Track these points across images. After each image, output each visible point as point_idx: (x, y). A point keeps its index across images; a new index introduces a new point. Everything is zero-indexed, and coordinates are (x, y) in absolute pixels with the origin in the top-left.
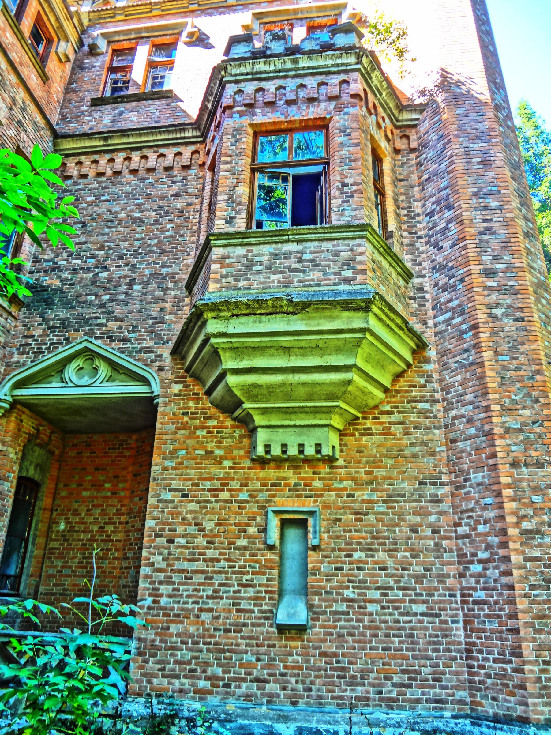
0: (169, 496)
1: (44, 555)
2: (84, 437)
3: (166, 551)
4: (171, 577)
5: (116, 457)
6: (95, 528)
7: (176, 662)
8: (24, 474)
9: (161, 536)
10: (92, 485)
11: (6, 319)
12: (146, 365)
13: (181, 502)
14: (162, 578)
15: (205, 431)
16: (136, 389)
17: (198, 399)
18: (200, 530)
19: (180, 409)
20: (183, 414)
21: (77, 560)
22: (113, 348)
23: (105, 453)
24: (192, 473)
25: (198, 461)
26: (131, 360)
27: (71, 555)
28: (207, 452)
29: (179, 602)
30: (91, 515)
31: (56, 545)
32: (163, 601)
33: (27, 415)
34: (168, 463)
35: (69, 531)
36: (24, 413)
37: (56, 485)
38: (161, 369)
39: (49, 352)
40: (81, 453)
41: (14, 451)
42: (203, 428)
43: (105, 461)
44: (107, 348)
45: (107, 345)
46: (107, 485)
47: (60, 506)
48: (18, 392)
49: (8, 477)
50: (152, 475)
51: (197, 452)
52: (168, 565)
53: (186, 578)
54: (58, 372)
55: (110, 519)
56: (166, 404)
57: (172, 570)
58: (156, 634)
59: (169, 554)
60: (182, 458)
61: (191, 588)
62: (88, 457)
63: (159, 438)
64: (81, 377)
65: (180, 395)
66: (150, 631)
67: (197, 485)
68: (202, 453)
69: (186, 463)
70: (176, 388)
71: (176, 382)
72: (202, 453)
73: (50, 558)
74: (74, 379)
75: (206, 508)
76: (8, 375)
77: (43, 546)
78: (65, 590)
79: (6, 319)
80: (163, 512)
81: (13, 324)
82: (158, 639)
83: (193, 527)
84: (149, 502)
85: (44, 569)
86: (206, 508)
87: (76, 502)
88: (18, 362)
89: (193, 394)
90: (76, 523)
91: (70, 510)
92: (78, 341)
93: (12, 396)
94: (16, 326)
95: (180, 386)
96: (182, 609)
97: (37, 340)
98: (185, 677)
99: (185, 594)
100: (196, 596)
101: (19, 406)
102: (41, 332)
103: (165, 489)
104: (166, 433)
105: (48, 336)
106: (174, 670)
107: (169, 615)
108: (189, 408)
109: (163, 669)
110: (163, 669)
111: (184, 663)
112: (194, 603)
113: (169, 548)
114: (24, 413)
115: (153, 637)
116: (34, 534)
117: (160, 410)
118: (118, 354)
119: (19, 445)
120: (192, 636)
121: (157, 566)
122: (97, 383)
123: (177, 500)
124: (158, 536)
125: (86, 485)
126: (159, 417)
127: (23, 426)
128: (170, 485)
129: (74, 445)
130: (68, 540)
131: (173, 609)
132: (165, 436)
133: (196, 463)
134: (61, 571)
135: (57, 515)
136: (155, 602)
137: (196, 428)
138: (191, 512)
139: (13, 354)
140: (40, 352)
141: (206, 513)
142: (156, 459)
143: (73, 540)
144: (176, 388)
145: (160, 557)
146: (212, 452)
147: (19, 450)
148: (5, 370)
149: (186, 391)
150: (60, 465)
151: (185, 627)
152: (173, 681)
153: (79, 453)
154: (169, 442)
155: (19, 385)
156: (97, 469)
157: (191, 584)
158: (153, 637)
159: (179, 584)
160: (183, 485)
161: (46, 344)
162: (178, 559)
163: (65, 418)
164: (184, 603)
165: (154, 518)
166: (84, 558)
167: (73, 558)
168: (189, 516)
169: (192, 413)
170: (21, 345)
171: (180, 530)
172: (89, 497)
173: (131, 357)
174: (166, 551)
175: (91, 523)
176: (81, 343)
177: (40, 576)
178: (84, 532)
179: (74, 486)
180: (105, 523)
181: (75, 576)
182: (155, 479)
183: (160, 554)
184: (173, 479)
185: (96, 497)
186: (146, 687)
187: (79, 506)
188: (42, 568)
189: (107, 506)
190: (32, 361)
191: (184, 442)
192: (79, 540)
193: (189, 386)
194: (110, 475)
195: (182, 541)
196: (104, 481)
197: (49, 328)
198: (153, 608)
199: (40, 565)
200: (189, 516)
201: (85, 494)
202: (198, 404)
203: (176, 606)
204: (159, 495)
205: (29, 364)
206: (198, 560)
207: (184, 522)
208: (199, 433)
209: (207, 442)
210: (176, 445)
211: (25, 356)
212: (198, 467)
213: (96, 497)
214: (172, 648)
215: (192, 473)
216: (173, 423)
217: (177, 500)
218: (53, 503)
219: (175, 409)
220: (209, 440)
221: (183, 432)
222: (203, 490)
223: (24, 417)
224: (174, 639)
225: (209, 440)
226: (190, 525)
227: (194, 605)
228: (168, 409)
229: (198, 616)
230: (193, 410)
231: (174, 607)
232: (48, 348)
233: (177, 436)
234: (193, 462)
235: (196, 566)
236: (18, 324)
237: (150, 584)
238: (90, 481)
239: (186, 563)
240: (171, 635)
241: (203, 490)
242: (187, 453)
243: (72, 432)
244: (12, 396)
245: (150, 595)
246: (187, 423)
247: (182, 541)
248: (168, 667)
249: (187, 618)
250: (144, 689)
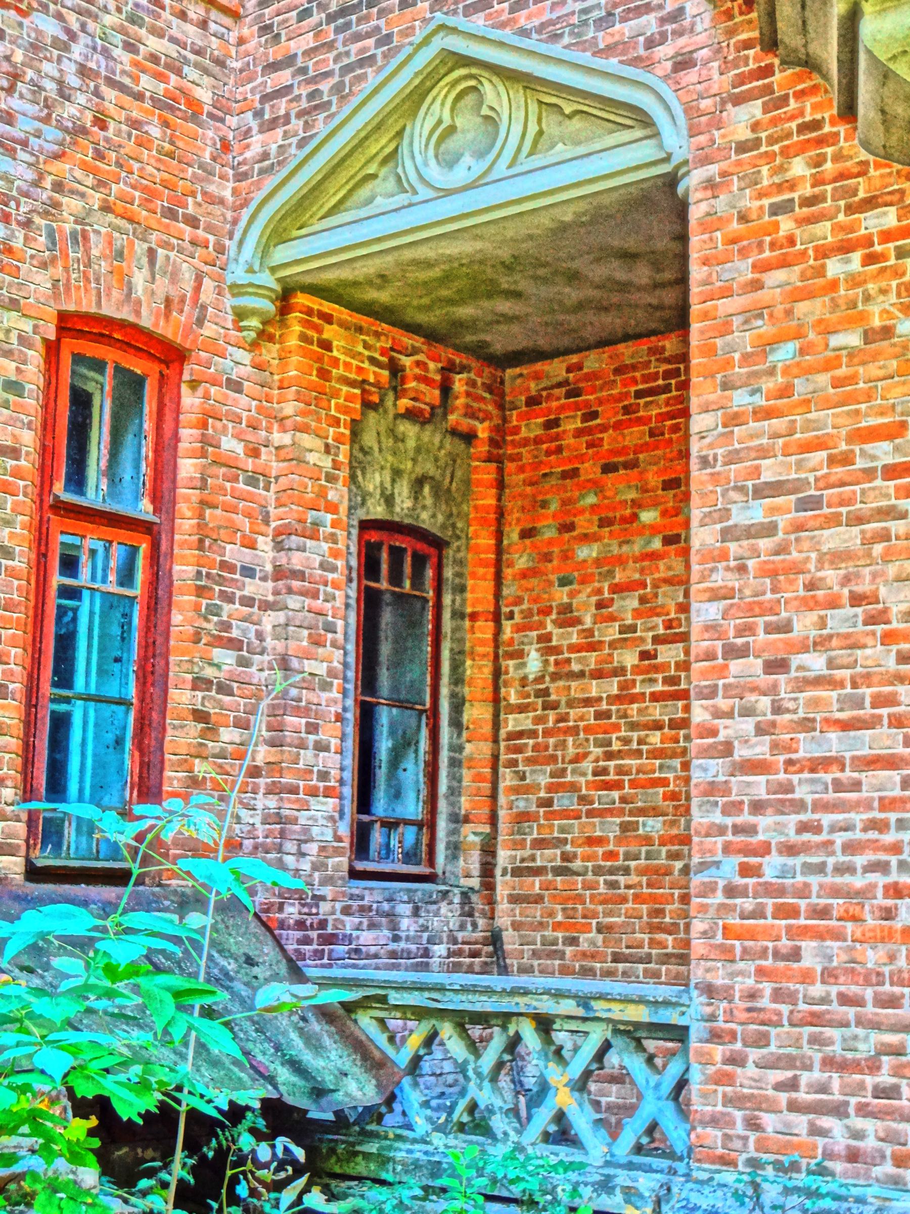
0: (756, 513)
1: (495, 758)
2: (557, 369)
3: (765, 703)
4: (788, 788)
5: (662, 417)
6: (629, 658)
7: (829, 1063)
8: (378, 511)
9: (742, 652)
10: (603, 523)
11: (203, 24)
12: (635, 62)
13: (799, 527)
14: (762, 793)
15: (856, 257)
16: (615, 161)
17: (821, 142)
18: (871, 620)
19: (760, 195)
20: (776, 210)
21: (588, 765)
22: (524, 33)
23: (627, 410)
24: (829, 421)
25: (843, 371)
26: (585, 58)
27: (571, 751)
28: (869, 336)
29: (821, 869)
30: (612, 618)
31: (525, 721)
32: (772, 866)
33: (343, 325)
34: (741, 399)
35: (555, 677)
36: (328, 318)
37: (499, 535)
38: (683, 63)
39: (343, 99)
40: (555, 423)
41: (319, 444)
42: (845, 248)
43: (635, 435)
44: (506, 35)
45: (502, 25)
46: (648, 516)
47: (518, 601)
48: (281, 254)
49: (316, 524)
50: (696, 448)
51: (836, 341)
52: (775, 747)
53: (838, 786)
54: (385, 161)
55: (669, 625)
56: (710, 185)
57: (790, 762)
58: (761, 972)
59: (777, 709)
60: (786, 371)
61: (858, 818)
62: (579, 433)
63: (705, 316)
64: (450, 162)
65: (757, 143)
66: (741, 965)
67: (846, 459)
68: (852, 339)
69: (801, 387)
70: (742, 119)
71: (738, 100)
72: (852, 339)
73: (513, 763)
74: (434, 172)
75: (885, 536)
76: (245, 203)
77: (487, 729)
78: (566, 857)
79: (203, 24)
80: (742, 569)
81: (233, 37)
82: (767, 988)
83: (850, 611)
84: (695, 544)
85: (502, 800)
86: (885, 536)
87: (564, 582)
88: (265, 156)
89: (803, 128)
90: (573, 648)
91: (546, 612)
92: (417, 38)
93: (273, 270)
94: (241, 41)
95: (755, 109)
96: (836, 892)
97: (303, 71)
98: (863, 1111)
99: (840, 838)
100: (875, 846)
101: (302, 299)
102: (308, 41)
103: (742, 489)
104: (726, 293)
105: (330, 46)
106: (823, 1088)
107: (794, 912)
108: (792, 185)
109: (792, 1085)
110: (792, 1085)
111: (855, 1066)
112: (872, 867)
113: (773, 690)
114: (328, 318)
115: (750, 982)
116: (453, 695)
117: (696, 213)
118: (543, 48)
119: (337, 422)
120: (874, 978)
121: (741, 753)
122: (501, 170)
123: (782, 521)
124: (734, 652)
125: (585, 523)
126: (695, 240)
127: (335, 362)
128: (756, 472)
129: (533, 401)
130: (555, 706)
131: (803, 892)
132: (725, 306)
133: (837, 383)
134: (548, 803)
135: (519, 629)
136: (746, 870)
137: (823, 253)
138: (837, 557)
139: (247, 133)
140: (317, 106)
141: (887, 558)
142: (701, 393)
143: (570, 704)
144: (742, 119)
145: (747, 725)
146: (887, 332)
147: (339, 439)
148: (235, 192)
149: (774, 122)
150: (500, 471)
151: (851, 949)
152: (826, 1122)
153: (551, 424)
154: (737, 321)
155: (278, 234)
156: (608, 469)
157: (855, 806)
158: (750, 982)
159: (819, 806)
160: (799, 465)
161: (328, 74)
162: (806, 725)
163: (465, 312)
164: (840, 870)
165: (715, 595)
166: (609, 756)
167: (577, 759)
168: (831, 575)
169: (808, 202)
170: (265, 98)
171: (804, 625)
172: (598, 562)
173: (581, 46)
174: (765, 703)
175: (613, 645)
176: (426, 41)
177: (493, 820)
178: (598, 674)
179: (550, 534)
180: (657, 640)
181: (590, 814)
182: (705, 462)
183: (748, 712)
184: (764, 453)
185: (621, 561)
186: (745, 1139)
187: (572, 595)
188: (494, 796)
189: (656, 586)
190: (301, 144)
191: (789, 313)
192: (588, 702)
193: (785, 100)
194: (654, 480)
195: (816, 663)
196: (637, 504)
197: (331, 18)
198: (742, 892)
199: (486, 786)
200: (831, 575)
201: (586, 552)
202: (818, 162)
203: (814, 881)
204: (726, 514)
205: (296, 155)
206: (871, 723)
207: (816, 599)
208: (834, 267)
209: (867, 298)
210: (763, 327)
211: (280, 131)
212: (846, 393)
213: (621, 561)
214: (815, 1019)
215: (829, 421)
216: (744, 253)
217: (782, 521)
218: (498, 595)
219: (748, 202)
220: (872, 287)
221: (779, 276)
222: (869, 474)
223: (330, 332)
224: (817, 990)
225: (872, 287)
226: (833, 603)
227: (872, 877)
228: (721, 203)
229: (888, 914)
230: (807, 190)
231: (807, 885)
232: (338, 89)
233: (763, 296)
234: (823, 379)
235: (865, 743)
236: (246, 31)
237: (725, 813)
238: (594, 508)
239: (833, 736)
240: (806, 977)
241: (869, 474)
242: (802, 352)
243: (516, 358)
244: (273, 270)
245: (728, 849)
246: (791, 241)
247: (816, 663)
248: (805, 1078)
249: (855, 919)
250: (738, 1144)
